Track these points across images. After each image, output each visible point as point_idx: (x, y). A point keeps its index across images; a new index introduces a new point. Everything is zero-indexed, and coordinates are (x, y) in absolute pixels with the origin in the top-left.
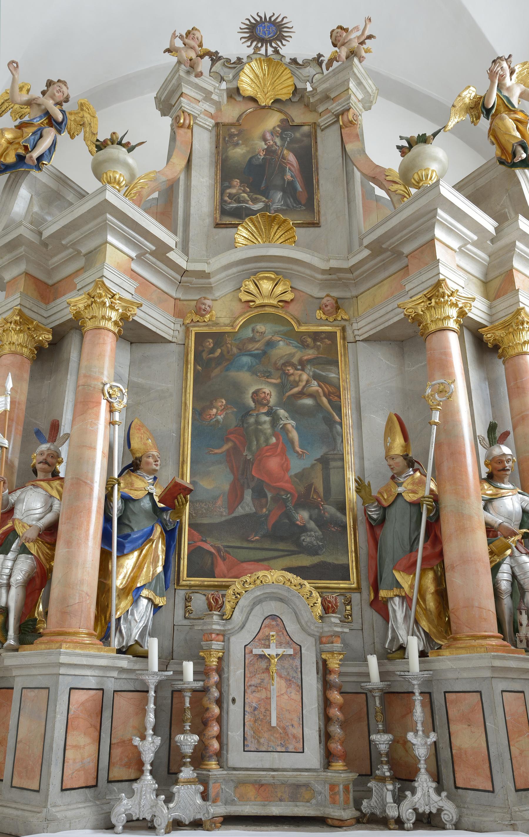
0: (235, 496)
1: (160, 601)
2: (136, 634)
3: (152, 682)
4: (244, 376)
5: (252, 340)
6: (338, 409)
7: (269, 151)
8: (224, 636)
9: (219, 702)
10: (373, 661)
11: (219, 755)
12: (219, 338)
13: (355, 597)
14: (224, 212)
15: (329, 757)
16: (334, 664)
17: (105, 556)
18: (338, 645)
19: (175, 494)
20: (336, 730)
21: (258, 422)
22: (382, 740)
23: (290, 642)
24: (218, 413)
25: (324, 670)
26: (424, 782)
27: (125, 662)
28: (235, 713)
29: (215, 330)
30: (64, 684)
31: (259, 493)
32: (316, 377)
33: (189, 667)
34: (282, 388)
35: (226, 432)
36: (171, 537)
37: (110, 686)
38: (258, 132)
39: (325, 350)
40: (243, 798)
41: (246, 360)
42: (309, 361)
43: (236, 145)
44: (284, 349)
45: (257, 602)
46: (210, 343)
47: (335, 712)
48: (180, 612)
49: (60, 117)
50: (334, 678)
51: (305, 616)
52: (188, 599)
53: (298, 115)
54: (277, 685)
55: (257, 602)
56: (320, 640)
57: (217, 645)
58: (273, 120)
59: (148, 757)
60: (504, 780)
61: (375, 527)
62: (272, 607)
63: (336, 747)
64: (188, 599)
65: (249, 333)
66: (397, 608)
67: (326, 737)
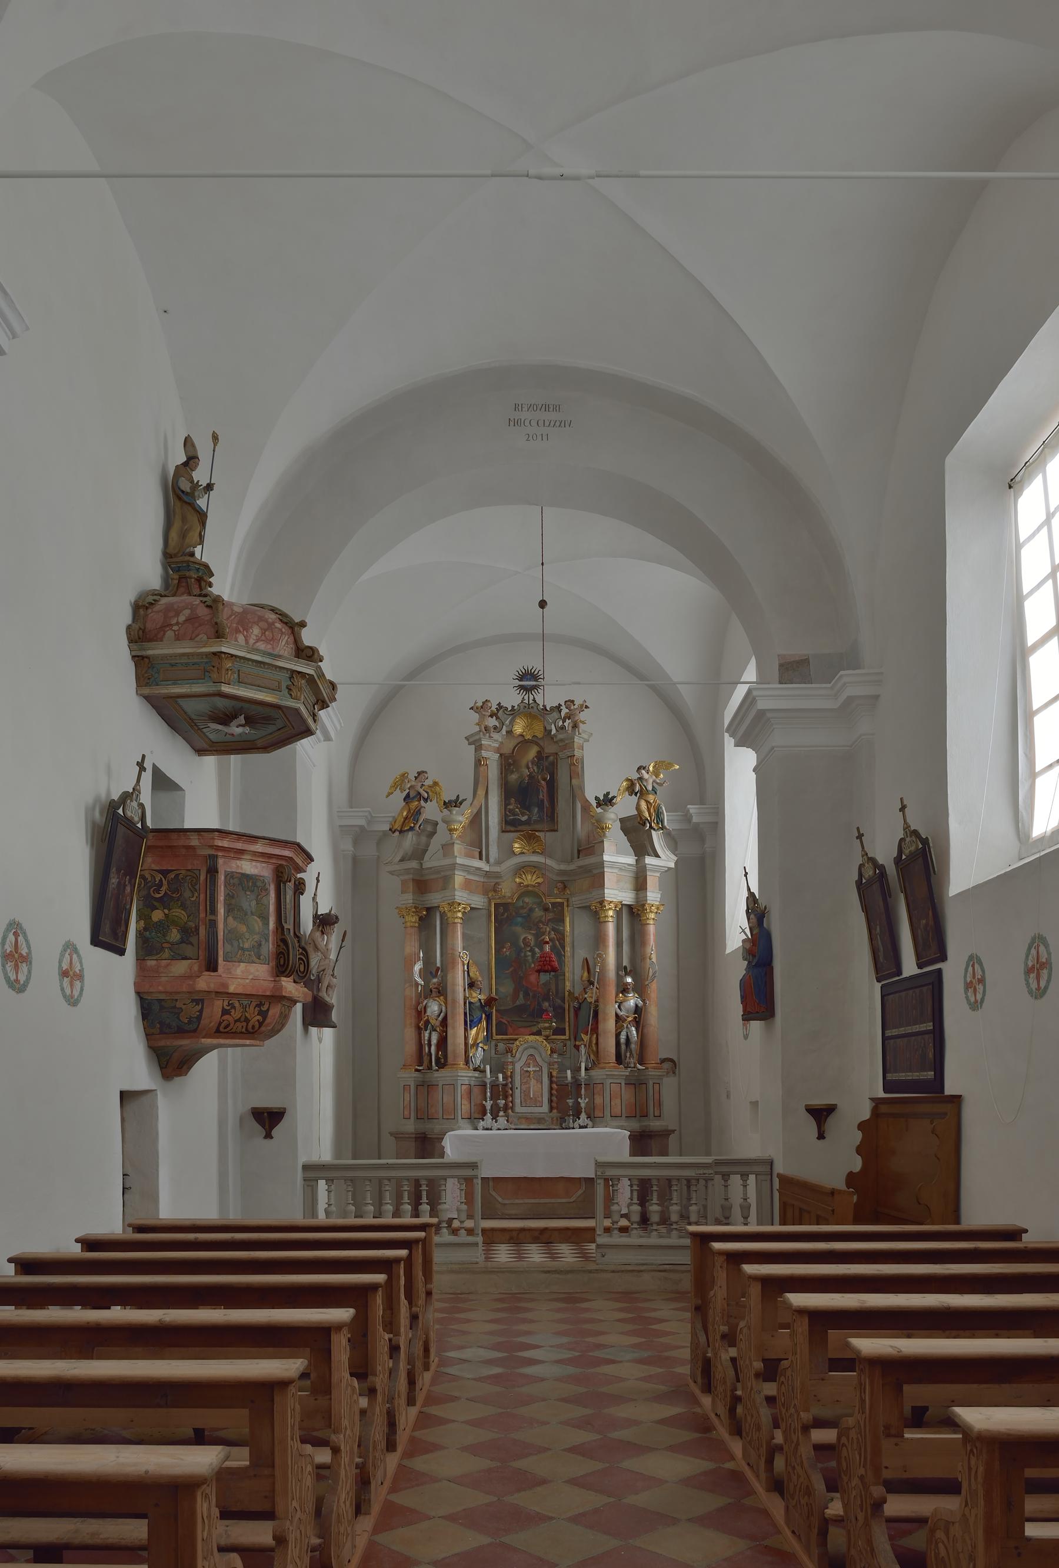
0: (515, 996)
1: (486, 1048)
2: (478, 1063)
3: (488, 1081)
4: (518, 929)
5: (522, 907)
6: (563, 947)
7: (530, 776)
8: (513, 1063)
9: (511, 1089)
10: (569, 1072)
11: (512, 1108)
12: (506, 906)
13: (568, 1043)
14: (507, 823)
15: (551, 1109)
16: (554, 1074)
17: (466, 1030)
18: (556, 1066)
19: (490, 1001)
20: (554, 1098)
21: (526, 956)
22: (570, 1102)
23: (538, 1065)
24: (506, 951)
25: (551, 1076)
26: (583, 1116)
27: (477, 1074)
28: (517, 1092)
29: (503, 901)
30: (460, 1082)
31: (526, 994)
32: (553, 929)
33: (500, 1076)
34: (537, 936)
35: (509, 964)
36: (489, 1018)
37: (472, 1083)
38: (524, 762)
39: (557, 914)
40: (521, 1124)
41: (519, 919)
42: (549, 920)
43: (512, 772)
44: (538, 913)
45: (526, 1049)
46: (501, 910)
47: (554, 1092)
48: (493, 1051)
49: (426, 795)
50: (554, 1079)
51: (544, 1055)
52: (496, 1046)
53: (550, 749)
54: (533, 1082)
55: (526, 1049)
56: (549, 1064)
57: (510, 1067)
58: (532, 753)
59: (488, 1108)
60: (607, 1113)
61: (577, 1011)
62: (531, 1051)
63: (554, 1105)
64: (496, 1046)
65: (521, 904)
66: (583, 1049)
67: (551, 1101)
